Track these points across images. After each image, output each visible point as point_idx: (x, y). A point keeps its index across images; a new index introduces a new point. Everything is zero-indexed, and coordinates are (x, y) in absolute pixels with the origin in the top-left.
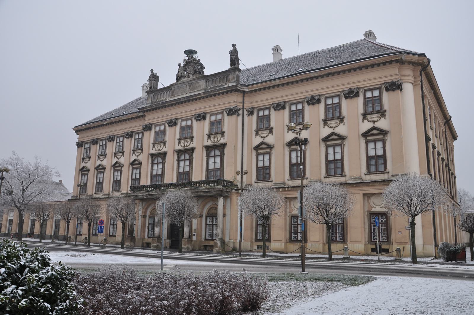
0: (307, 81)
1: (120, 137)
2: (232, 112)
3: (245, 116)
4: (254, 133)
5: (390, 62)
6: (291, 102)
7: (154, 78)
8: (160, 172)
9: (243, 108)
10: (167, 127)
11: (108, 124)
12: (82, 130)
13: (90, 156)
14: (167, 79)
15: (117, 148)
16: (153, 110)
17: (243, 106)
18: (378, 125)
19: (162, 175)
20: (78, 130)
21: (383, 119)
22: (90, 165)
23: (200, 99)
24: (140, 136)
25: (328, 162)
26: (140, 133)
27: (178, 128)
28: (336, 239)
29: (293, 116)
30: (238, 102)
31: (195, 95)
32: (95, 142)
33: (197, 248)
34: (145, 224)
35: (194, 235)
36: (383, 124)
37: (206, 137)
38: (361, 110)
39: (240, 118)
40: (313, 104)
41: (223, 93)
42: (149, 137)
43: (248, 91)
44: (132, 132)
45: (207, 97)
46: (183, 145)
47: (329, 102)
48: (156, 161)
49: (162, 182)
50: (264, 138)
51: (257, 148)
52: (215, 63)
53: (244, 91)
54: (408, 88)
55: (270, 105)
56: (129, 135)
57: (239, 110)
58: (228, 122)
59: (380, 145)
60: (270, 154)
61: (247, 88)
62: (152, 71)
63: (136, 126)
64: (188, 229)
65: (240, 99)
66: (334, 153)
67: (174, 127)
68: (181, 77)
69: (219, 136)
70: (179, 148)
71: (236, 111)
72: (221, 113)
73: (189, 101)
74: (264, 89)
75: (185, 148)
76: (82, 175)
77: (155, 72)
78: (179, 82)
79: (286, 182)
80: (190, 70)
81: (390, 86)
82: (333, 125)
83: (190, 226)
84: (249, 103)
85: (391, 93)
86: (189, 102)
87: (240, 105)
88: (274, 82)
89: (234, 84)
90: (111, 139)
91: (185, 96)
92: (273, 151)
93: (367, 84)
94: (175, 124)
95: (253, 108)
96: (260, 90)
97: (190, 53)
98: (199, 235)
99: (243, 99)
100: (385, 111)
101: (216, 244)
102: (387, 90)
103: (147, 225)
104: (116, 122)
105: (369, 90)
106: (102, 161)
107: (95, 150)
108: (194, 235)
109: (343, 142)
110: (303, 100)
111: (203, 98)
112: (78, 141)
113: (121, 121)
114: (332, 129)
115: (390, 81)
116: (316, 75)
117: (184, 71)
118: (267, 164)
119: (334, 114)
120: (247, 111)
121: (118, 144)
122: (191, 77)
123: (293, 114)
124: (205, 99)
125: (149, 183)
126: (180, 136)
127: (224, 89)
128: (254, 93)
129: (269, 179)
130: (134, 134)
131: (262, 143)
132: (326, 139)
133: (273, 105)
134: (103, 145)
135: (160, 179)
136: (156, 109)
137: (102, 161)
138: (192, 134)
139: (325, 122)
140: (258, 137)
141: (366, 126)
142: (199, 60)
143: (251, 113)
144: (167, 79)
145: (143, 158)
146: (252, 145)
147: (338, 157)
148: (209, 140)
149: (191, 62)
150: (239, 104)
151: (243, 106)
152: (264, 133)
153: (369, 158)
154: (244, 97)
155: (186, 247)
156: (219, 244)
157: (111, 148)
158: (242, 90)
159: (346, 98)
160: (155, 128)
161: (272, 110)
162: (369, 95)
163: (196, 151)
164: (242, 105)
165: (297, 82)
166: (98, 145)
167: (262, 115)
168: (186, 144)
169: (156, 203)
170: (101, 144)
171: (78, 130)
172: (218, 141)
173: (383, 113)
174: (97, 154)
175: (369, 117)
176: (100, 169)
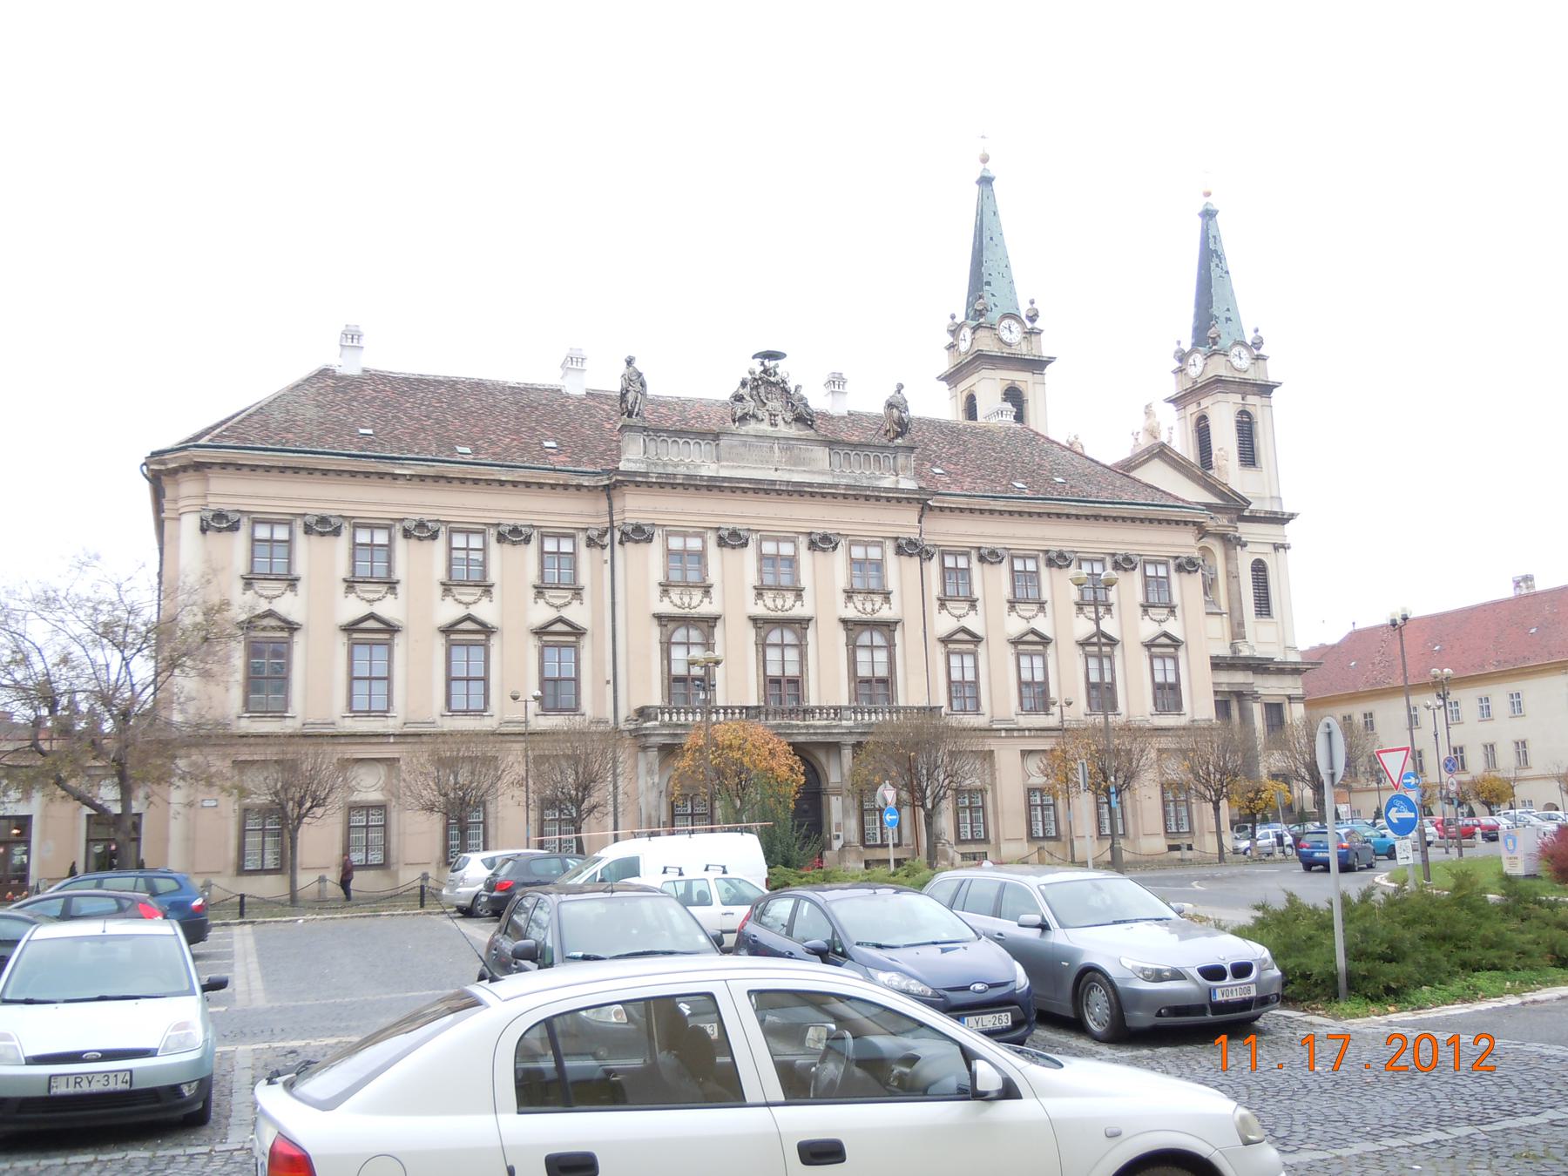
2: (905, 548)
3: (617, 546)
5: (1186, 523)
9: (612, 527)
17: (612, 521)
18: (567, 613)
25: (1021, 684)
37: (657, 591)
38: (343, 570)
46: (770, 604)
58: (899, 573)
62: (900, 387)
69: (878, 599)
75: (780, 614)
79: (439, 721)
85: (507, 547)
93: (1149, 551)
99: (611, 507)
102: (308, 530)
109: (392, 639)
111: (845, 496)
119: (467, 578)
124: (785, 496)
127: (878, 489)
142: (766, 384)
147: (969, 676)
148: (850, 605)
151: (612, 521)
165: (268, 469)
168: (686, 600)
171: (163, 473)
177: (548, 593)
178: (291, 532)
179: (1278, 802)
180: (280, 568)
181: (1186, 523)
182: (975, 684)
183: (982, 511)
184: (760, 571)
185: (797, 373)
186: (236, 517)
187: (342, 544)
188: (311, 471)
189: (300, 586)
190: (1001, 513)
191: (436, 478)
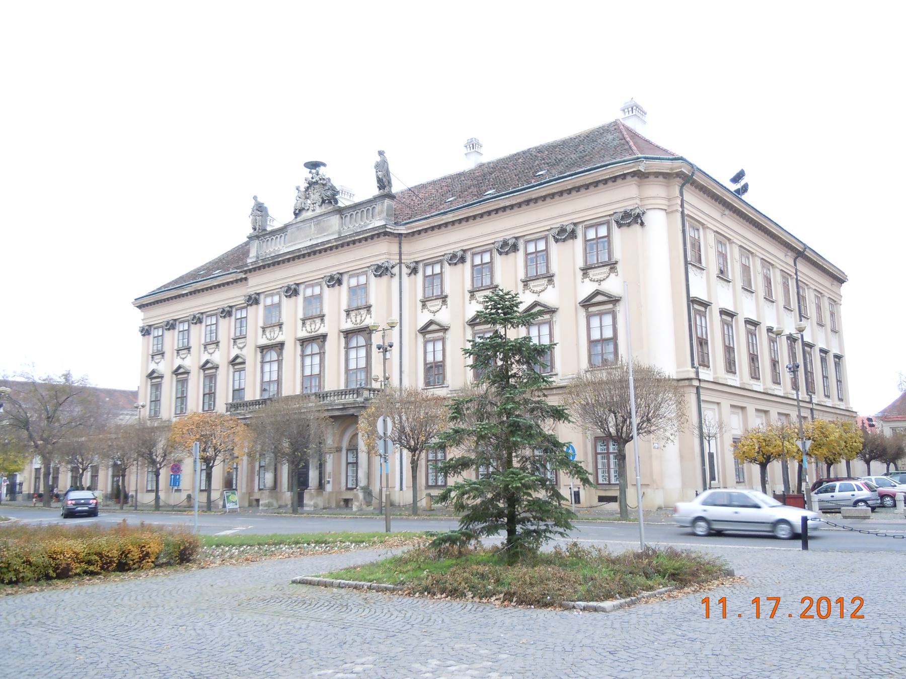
0: (528, 205)
1: (211, 315)
2: (381, 271)
3: (404, 276)
4: (420, 305)
5: (624, 176)
6: (474, 250)
7: (260, 209)
8: (316, 371)
9: (400, 263)
10: (284, 299)
11: (191, 293)
12: (147, 305)
13: (495, 284)
14: (281, 214)
15: (208, 336)
16: (259, 268)
17: (400, 259)
19: (279, 382)
20: (143, 305)
21: (612, 275)
22: (164, 367)
23: (331, 248)
24: (186, 327)
26: (437, 262)
27: (300, 298)
28: (609, 481)
29: (592, 249)
30: (390, 254)
31: (323, 243)
32: (171, 326)
33: (334, 505)
34: (253, 467)
35: (329, 482)
36: (612, 285)
39: (396, 280)
40: (507, 253)
41: (366, 239)
42: (256, 316)
43: (408, 234)
44: (231, 307)
45: (342, 245)
47: (531, 248)
48: (308, 352)
49: (320, 388)
50: (434, 312)
51: (424, 331)
52: (357, 186)
53: (401, 234)
54: (656, 220)
55: (610, 215)
56: (227, 313)
57: (393, 267)
58: (377, 289)
59: (608, 320)
60: (443, 340)
61: (403, 228)
62: (255, 198)
63: (234, 296)
64: (317, 472)
65: (395, 248)
66: (601, 327)
67: (294, 298)
68: (300, 211)
70: (303, 334)
71: (387, 269)
72: (365, 273)
73: (315, 253)
74: (433, 228)
76: (426, 343)
77: (260, 200)
78: (299, 219)
80: (315, 196)
81: (623, 218)
82: (538, 289)
83: (321, 467)
84: (410, 254)
86: (378, 237)
87: (395, 259)
88: (444, 217)
89: (382, 223)
90: (197, 320)
91: (309, 243)
92: (449, 335)
94: (296, 293)
95: (417, 262)
96: (426, 230)
97: (313, 165)
98: (337, 482)
99: (400, 247)
100: (616, 263)
101: (356, 496)
103: (257, 468)
104: (203, 290)
105: (591, 226)
106: (157, 363)
107: (171, 340)
108: (329, 482)
110: (608, 218)
111: (337, 247)
112: (142, 325)
113: (211, 288)
114: (536, 295)
115: (622, 210)
116: (508, 203)
117: (307, 198)
118: (439, 358)
120: (408, 267)
121: (209, 328)
122: (319, 211)
123: (532, 259)
125: (298, 391)
126: (304, 314)
128: (416, 236)
129: (443, 383)
130: (234, 310)
131: (597, 293)
132: (587, 304)
133: (552, 232)
134: (433, 275)
135: (363, 377)
136: (264, 267)
137: (157, 363)
138: (321, 310)
139: (585, 270)
140: (425, 311)
141: (587, 289)
143: (414, 271)
144: (281, 214)
145: (250, 354)
146: (576, 299)
148: (349, 320)
149: (316, 183)
150: (392, 257)
151: (400, 259)
152: (434, 305)
153: (592, 343)
154: (400, 244)
155: (312, 503)
156: (361, 495)
157: (198, 335)
158: (396, 232)
159: (620, 225)
160: (265, 301)
161: (446, 264)
162: (591, 234)
163: (286, 346)
164: (398, 257)
165: (481, 215)
166: (176, 331)
167: (594, 237)
169: (357, 423)
170: (239, 316)
171: (143, 305)
172: (362, 322)
173: (612, 266)
174: (203, 342)
175: (591, 273)
176: (180, 373)
177: (428, 304)
178: (321, 289)
179: (457, 500)
180: (542, 270)
181: (624, 176)
182: (614, 339)
183: (439, 227)
184: (526, 267)
185: (331, 173)
186: (511, 242)
187: (578, 244)
188: (596, 184)
189: (619, 267)
190: (453, 223)
191: (528, 202)
